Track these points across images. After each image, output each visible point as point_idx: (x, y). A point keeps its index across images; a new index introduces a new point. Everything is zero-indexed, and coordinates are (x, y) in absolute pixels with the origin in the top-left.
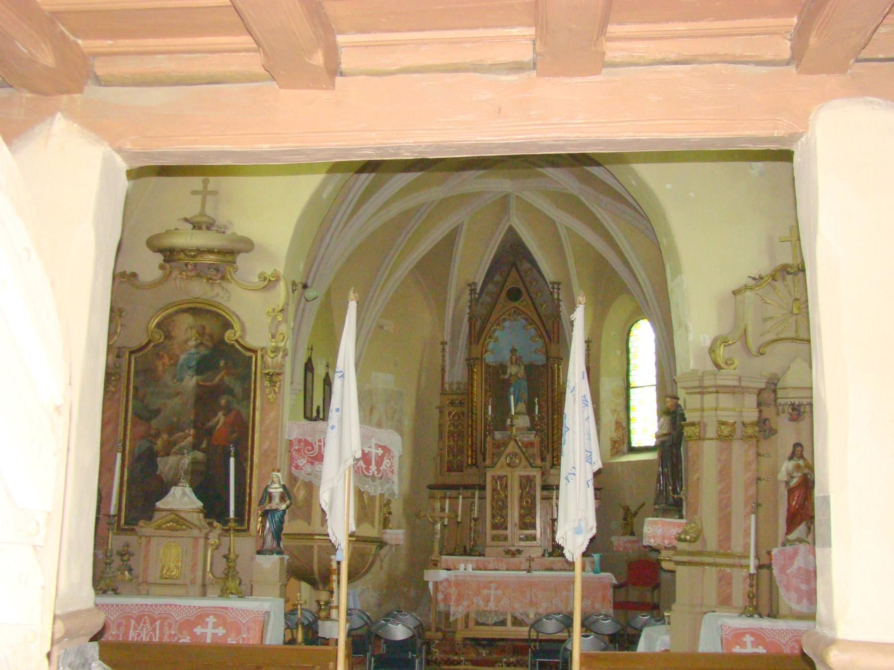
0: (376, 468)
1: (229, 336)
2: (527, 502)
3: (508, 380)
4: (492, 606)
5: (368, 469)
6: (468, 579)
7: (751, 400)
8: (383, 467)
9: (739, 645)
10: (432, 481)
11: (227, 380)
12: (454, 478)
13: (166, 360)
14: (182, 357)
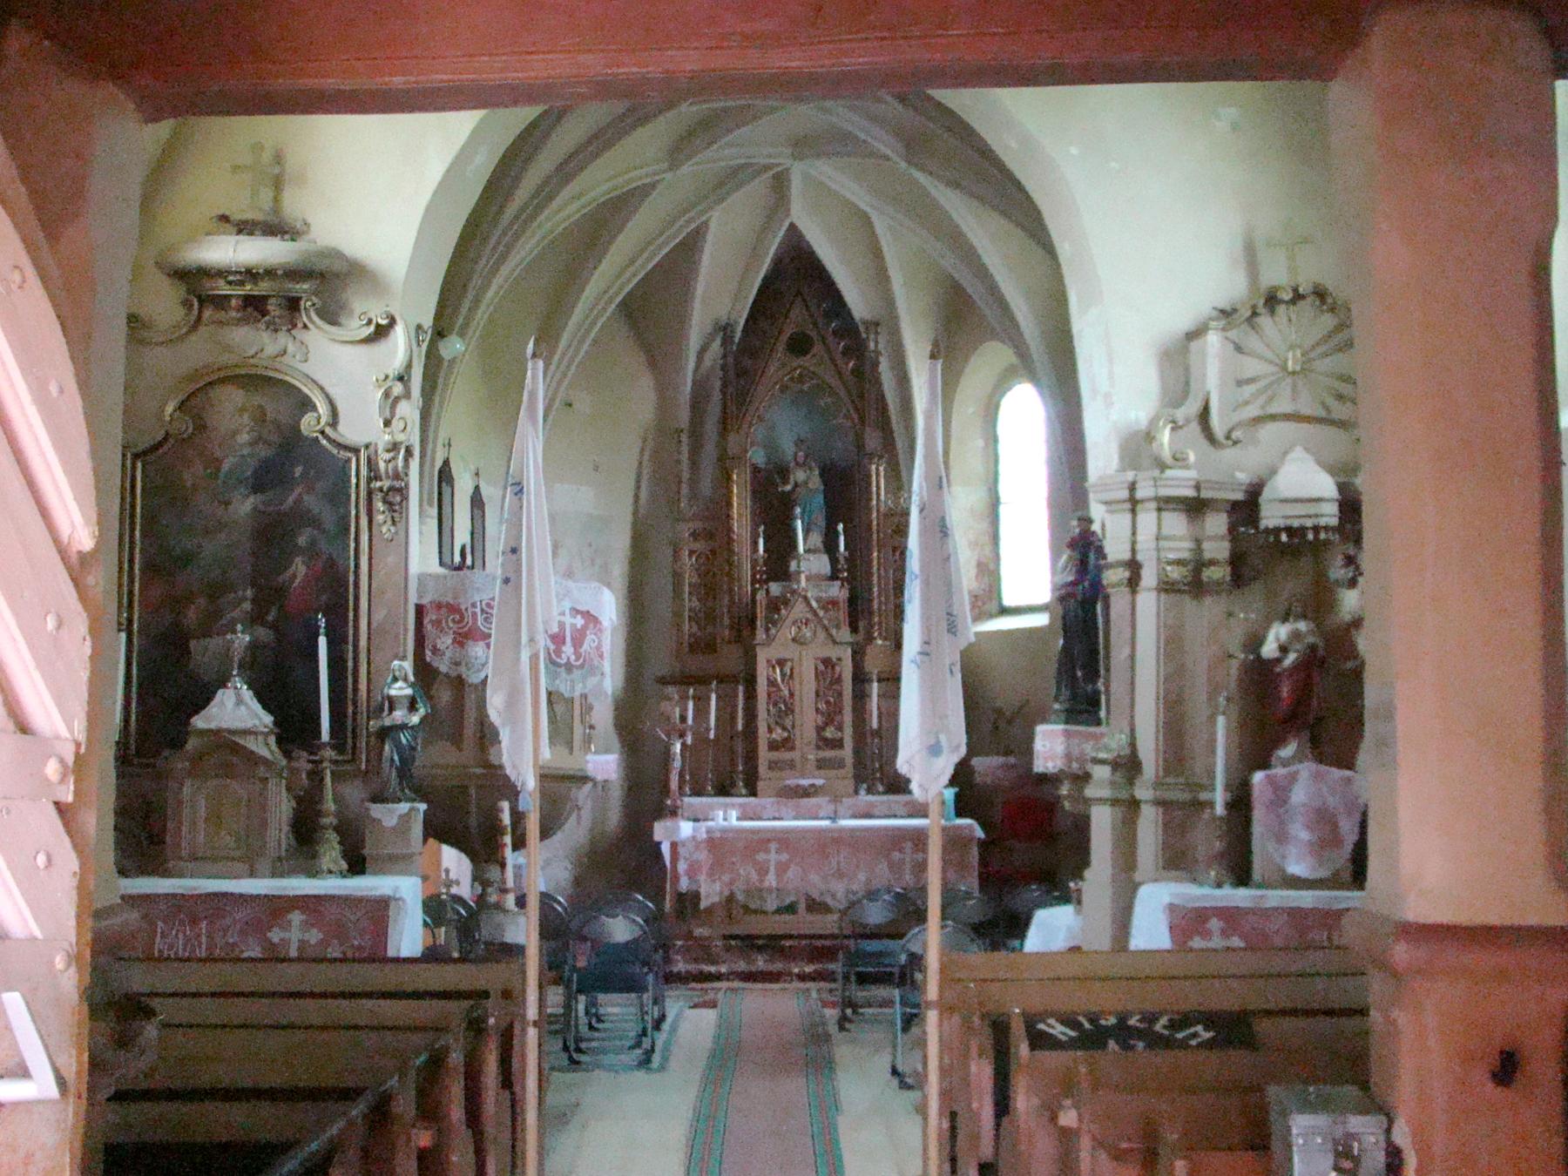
0: (572, 650)
1: (308, 424)
2: (828, 703)
4: (771, 880)
5: (558, 652)
7: (1217, 523)
9: (1200, 934)
10: (664, 671)
11: (311, 501)
12: (696, 664)
13: (198, 468)
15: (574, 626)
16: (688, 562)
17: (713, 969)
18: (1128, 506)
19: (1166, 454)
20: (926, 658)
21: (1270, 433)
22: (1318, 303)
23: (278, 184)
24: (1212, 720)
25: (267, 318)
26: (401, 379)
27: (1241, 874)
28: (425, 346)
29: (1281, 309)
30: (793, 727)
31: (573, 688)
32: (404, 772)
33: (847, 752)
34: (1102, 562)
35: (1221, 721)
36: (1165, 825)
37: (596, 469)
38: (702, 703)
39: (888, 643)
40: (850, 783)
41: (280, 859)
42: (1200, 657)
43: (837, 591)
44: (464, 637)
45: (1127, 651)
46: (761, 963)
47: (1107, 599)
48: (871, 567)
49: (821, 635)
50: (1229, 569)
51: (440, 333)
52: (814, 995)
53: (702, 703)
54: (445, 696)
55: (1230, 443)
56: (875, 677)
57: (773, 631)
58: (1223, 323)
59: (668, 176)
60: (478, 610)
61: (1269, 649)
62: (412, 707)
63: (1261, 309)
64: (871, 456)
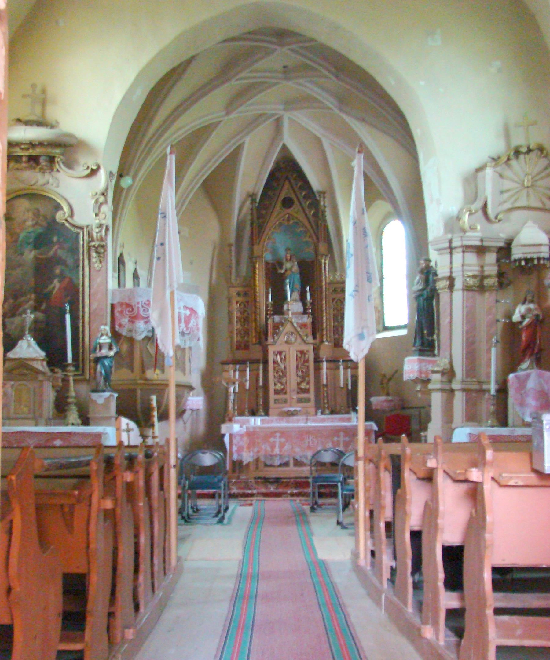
1: (59, 217)
2: (302, 372)
3: (284, 273)
4: (277, 451)
6: (258, 430)
7: (491, 258)
8: (190, 325)
10: (225, 358)
11: (60, 252)
12: (241, 354)
14: (22, 235)
15: (185, 314)
16: (235, 307)
17: (249, 492)
18: (448, 251)
19: (466, 226)
20: (356, 293)
21: (516, 215)
22: (539, 153)
23: (44, 103)
24: (489, 351)
25: (40, 167)
26: (103, 194)
27: (503, 422)
28: (114, 182)
29: (522, 157)
30: (286, 383)
31: (185, 344)
32: (107, 379)
33: (312, 395)
34: (435, 278)
35: (493, 350)
36: (467, 402)
37: (191, 263)
38: (243, 372)
39: (330, 344)
40: (313, 410)
41: (49, 419)
42: (483, 320)
43: (307, 319)
44: (133, 319)
45: (448, 320)
46: (272, 489)
47: (438, 295)
48: (322, 307)
49: (299, 340)
50: (497, 280)
51: (121, 176)
52: (298, 501)
53: (243, 372)
54: (125, 347)
55: (497, 221)
56: (324, 360)
57: (276, 338)
58: (493, 164)
59: (226, 118)
60: (140, 306)
61: (516, 317)
62: (110, 348)
63: (512, 157)
64: (322, 255)
